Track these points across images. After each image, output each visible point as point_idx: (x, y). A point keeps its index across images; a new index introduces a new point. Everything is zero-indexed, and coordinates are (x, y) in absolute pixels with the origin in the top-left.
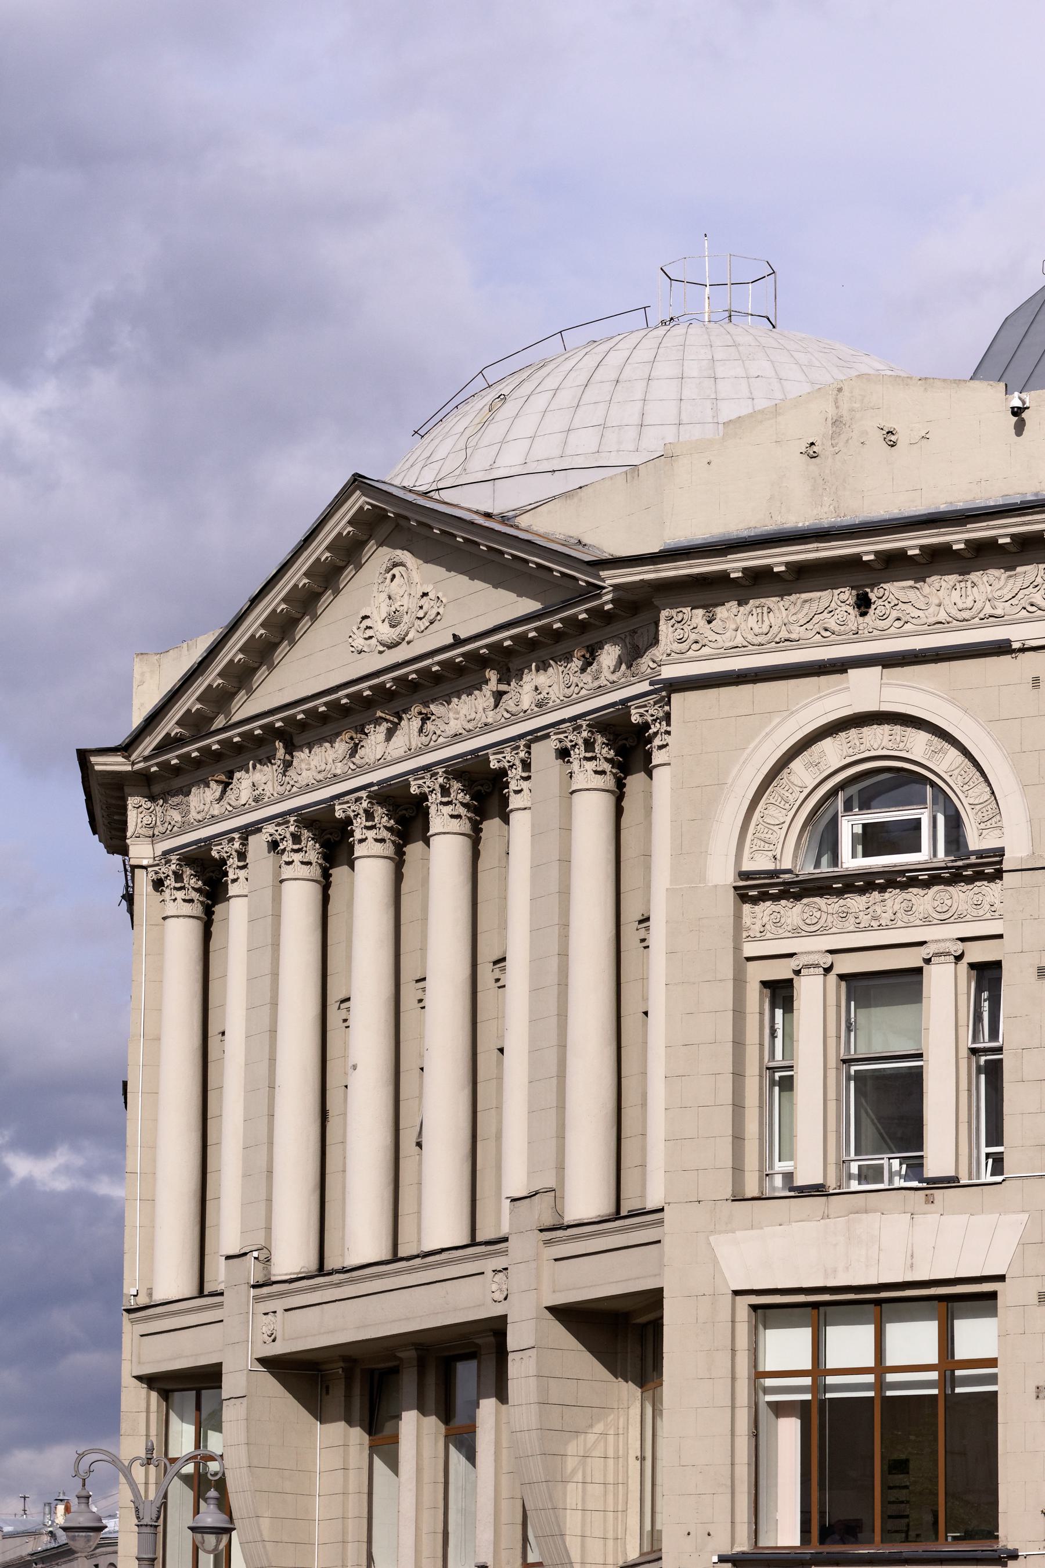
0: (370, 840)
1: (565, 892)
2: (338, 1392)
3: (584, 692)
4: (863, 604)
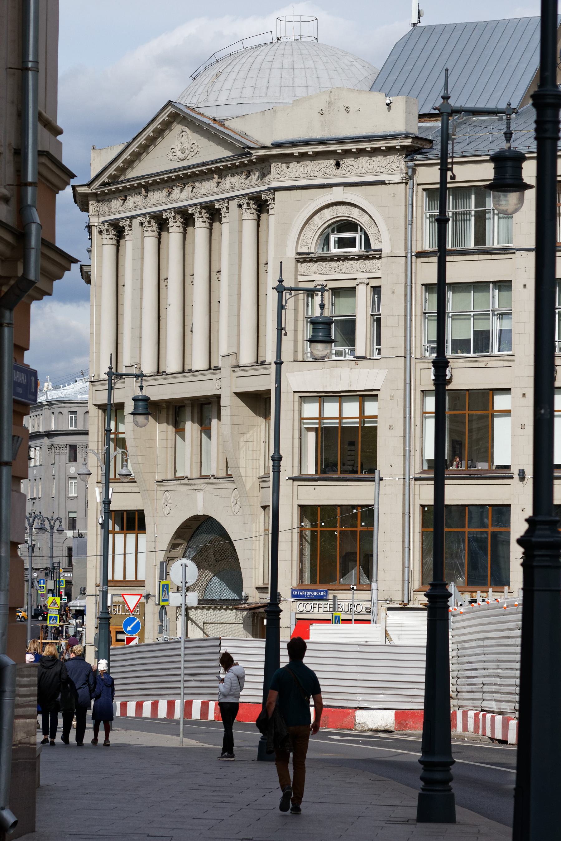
0: (175, 226)
1: (240, 253)
2: (164, 413)
3: (246, 186)
4: (338, 165)
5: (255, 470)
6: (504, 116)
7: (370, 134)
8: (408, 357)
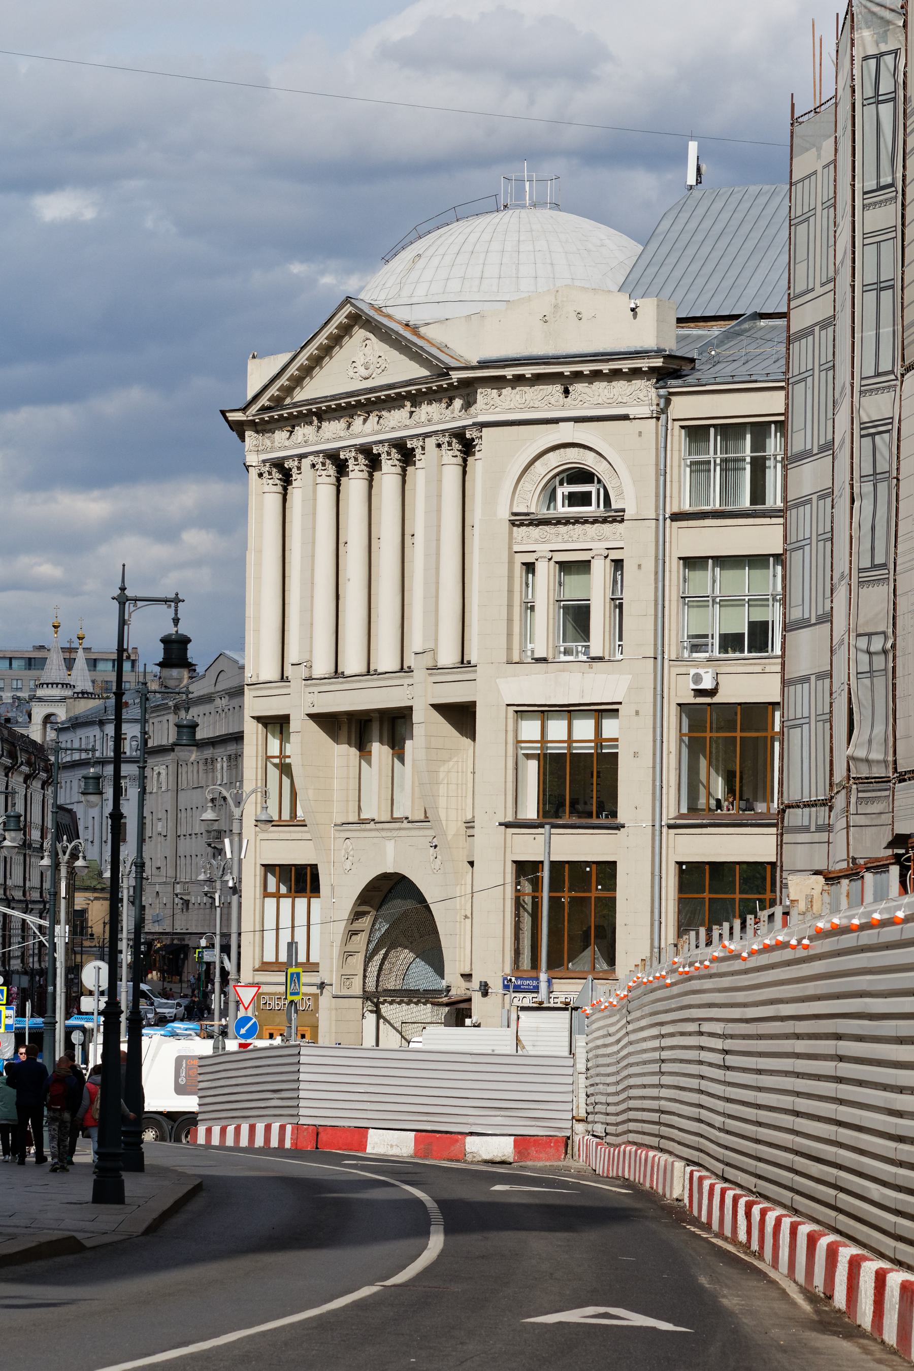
0: (356, 471)
1: (439, 511)
2: (345, 729)
3: (447, 418)
4: (566, 392)
5: (460, 811)
6: (173, 604)
7: (609, 350)
8: (659, 657)
